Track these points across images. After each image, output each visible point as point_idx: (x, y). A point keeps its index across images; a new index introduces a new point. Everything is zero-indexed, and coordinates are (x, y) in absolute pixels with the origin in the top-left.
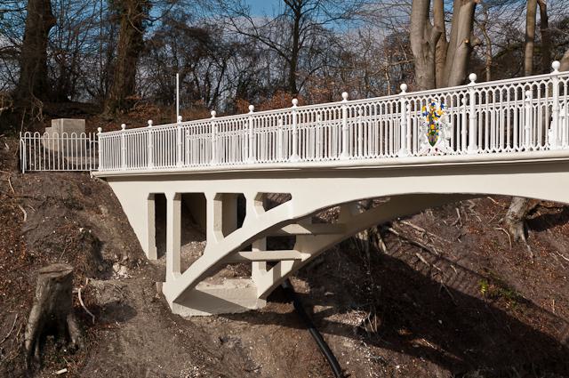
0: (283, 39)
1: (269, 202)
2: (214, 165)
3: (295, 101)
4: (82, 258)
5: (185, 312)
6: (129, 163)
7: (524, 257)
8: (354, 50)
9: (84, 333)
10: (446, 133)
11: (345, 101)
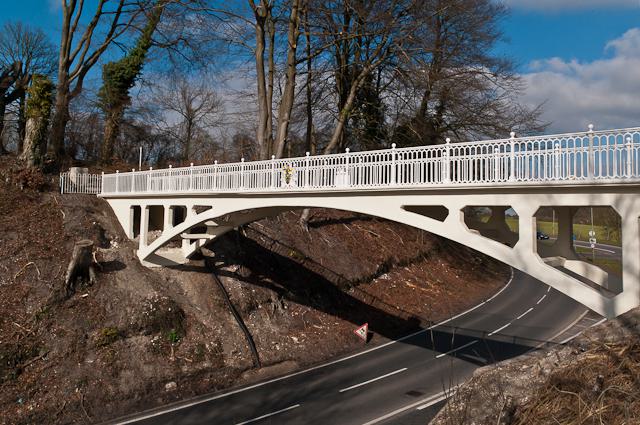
0: (182, 134)
1: (199, 209)
2: (170, 192)
3: (308, 153)
4: (95, 237)
5: (148, 265)
6: (120, 190)
7: (308, 239)
8: (218, 140)
9: (97, 276)
10: (294, 178)
11: (513, 138)
